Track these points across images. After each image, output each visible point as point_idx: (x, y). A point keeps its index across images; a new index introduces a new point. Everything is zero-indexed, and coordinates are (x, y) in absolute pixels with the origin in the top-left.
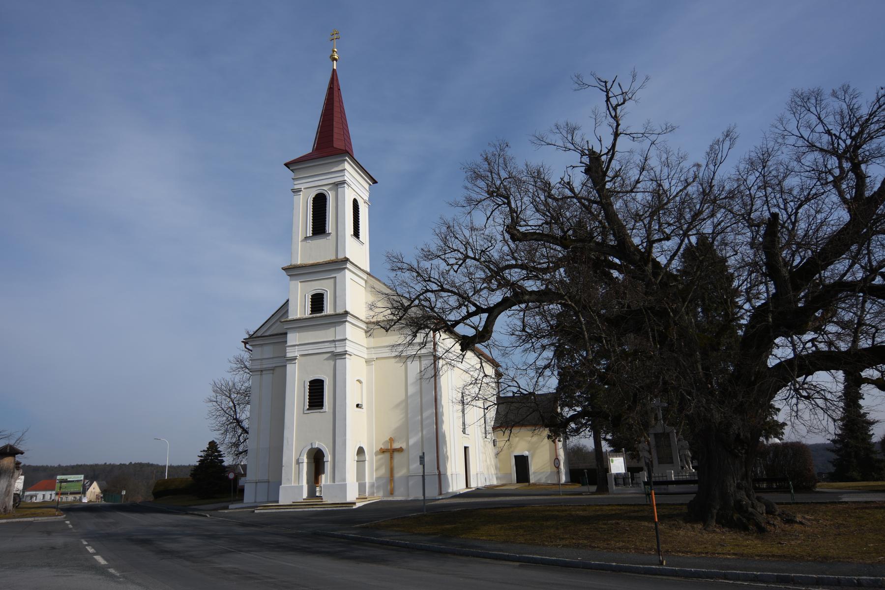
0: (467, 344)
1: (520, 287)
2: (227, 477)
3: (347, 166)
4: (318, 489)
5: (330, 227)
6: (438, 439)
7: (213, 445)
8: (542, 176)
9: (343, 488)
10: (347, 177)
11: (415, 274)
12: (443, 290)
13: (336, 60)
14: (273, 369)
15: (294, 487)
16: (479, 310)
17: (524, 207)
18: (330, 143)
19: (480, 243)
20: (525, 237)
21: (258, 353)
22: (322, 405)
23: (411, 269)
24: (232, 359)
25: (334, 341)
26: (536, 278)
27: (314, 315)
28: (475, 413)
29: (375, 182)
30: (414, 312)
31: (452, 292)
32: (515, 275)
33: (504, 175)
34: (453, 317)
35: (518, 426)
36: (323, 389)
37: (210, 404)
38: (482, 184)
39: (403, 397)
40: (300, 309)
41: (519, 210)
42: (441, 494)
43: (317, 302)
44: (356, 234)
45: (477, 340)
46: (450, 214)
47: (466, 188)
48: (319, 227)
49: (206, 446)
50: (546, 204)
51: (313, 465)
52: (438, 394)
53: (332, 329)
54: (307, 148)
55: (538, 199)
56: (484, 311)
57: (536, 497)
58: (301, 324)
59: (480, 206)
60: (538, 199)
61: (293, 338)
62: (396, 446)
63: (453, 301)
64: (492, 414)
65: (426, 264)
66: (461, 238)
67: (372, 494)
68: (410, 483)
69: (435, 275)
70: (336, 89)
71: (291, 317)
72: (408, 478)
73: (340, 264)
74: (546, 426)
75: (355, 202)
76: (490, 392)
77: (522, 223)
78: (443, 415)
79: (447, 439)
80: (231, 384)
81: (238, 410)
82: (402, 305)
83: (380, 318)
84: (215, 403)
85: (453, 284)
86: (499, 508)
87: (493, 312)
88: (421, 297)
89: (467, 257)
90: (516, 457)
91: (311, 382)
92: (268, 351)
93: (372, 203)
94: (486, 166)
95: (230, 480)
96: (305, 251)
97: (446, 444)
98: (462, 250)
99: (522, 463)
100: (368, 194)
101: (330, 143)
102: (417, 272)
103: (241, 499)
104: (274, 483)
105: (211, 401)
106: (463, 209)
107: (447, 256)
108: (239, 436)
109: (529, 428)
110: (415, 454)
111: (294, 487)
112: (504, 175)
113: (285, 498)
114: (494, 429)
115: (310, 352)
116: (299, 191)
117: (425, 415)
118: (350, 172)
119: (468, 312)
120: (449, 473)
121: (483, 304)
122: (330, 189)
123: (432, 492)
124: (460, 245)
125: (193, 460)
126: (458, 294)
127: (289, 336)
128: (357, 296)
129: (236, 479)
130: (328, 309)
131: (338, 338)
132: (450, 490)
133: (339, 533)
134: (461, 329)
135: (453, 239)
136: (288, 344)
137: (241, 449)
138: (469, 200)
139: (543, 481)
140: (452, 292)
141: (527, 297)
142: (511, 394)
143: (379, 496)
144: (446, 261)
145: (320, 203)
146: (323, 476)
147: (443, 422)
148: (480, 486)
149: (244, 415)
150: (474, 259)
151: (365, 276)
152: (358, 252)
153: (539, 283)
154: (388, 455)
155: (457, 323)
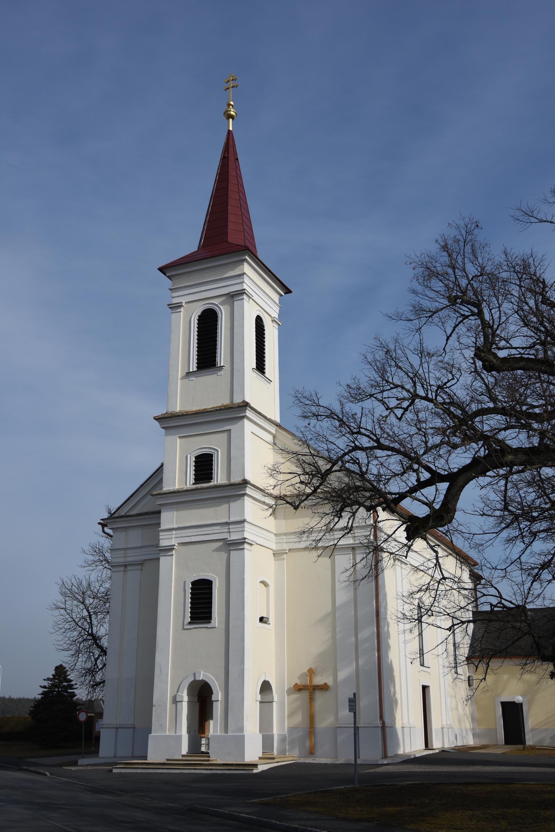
0: (416, 528)
1: (501, 443)
2: (76, 717)
3: (246, 268)
4: (203, 741)
5: (222, 358)
6: (381, 675)
7: (60, 671)
8: (532, 270)
9: (240, 741)
10: (247, 285)
11: (337, 423)
12: (381, 447)
13: (232, 117)
14: (142, 563)
15: (170, 737)
16: (436, 478)
17: (503, 319)
18: (225, 236)
19: (434, 375)
20: (510, 364)
21: (121, 540)
22: (210, 618)
23: (332, 415)
24: (87, 548)
25: (227, 524)
26: (527, 427)
27: (199, 486)
28: (435, 634)
29: (288, 291)
30: (337, 480)
31: (392, 449)
32: (489, 423)
33: (472, 270)
34: (395, 487)
35: (500, 657)
36: (211, 593)
37: (57, 612)
38: (437, 285)
39: (328, 608)
40: (180, 477)
41: (496, 323)
42: (385, 756)
43: (204, 466)
44: (260, 367)
45: (431, 523)
46: (390, 332)
47: (414, 292)
48: (207, 359)
49: (51, 673)
50: (538, 313)
51: (197, 705)
52: (382, 604)
53: (225, 506)
54: (190, 242)
55: (526, 308)
56: (442, 478)
57: (533, 769)
58: (181, 499)
59: (435, 319)
60: (526, 308)
61: (169, 519)
62: (318, 680)
63: (394, 463)
64: (464, 638)
65: (354, 408)
66: (407, 367)
67: (283, 752)
68: (340, 739)
69: (367, 424)
70: (231, 158)
71: (167, 487)
72: (335, 730)
73: (236, 410)
74: (545, 659)
75: (259, 321)
76: (456, 600)
77: (503, 343)
78: (388, 636)
79: (396, 674)
80: (84, 583)
81: (95, 622)
82: (318, 470)
83: (287, 490)
84: (62, 611)
85: (393, 437)
86: (471, 784)
87: (457, 480)
88: (347, 458)
89: (415, 396)
90: (503, 704)
91: (194, 583)
92: (135, 538)
93: (283, 321)
94: (445, 259)
95: (80, 723)
96: (189, 394)
97: (393, 681)
98: (408, 386)
99: (513, 713)
100: (277, 309)
101: (225, 236)
102: (340, 420)
103: (96, 752)
104: (140, 729)
105: (58, 608)
106: (409, 324)
107: (385, 394)
108: (96, 660)
109: (517, 661)
110: (346, 694)
111: (170, 737)
112: (472, 270)
113: (156, 754)
114: (468, 659)
115: (193, 539)
116: (179, 306)
117: (362, 635)
118: (251, 277)
119: (418, 480)
120: (398, 725)
121: (440, 466)
122: (222, 303)
123: (370, 754)
124: (406, 379)
125: (34, 692)
126: (405, 455)
127: (165, 516)
128: (259, 456)
129: (91, 722)
130: (219, 477)
131: (232, 519)
132: (401, 752)
133: (226, 810)
134: (411, 506)
135: (393, 369)
136: (163, 527)
137: (98, 678)
138: (418, 311)
139: (547, 743)
140: (392, 449)
141: (510, 457)
142: (487, 608)
143: (293, 756)
144: (384, 403)
145: (208, 323)
146: (211, 722)
147: (388, 647)
148: (447, 746)
149: (101, 631)
150: (426, 398)
151: (273, 429)
152: (263, 394)
153: (523, 436)
154: (305, 694)
155: (402, 496)
